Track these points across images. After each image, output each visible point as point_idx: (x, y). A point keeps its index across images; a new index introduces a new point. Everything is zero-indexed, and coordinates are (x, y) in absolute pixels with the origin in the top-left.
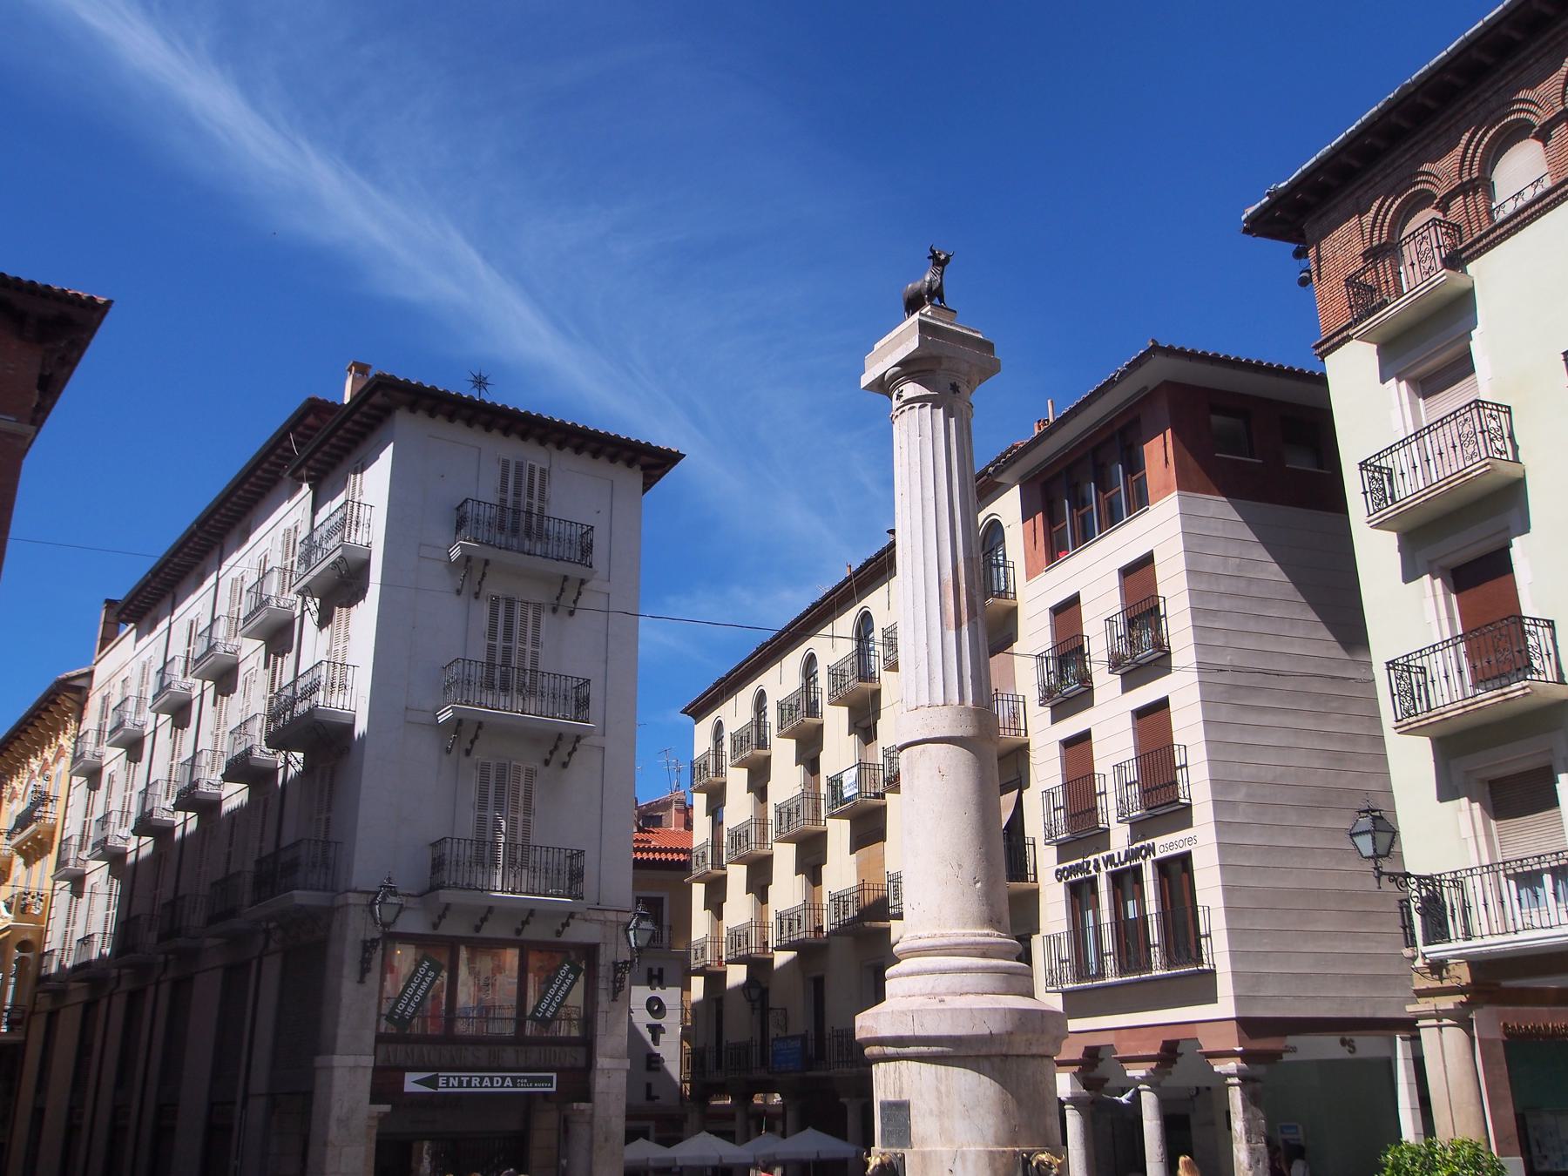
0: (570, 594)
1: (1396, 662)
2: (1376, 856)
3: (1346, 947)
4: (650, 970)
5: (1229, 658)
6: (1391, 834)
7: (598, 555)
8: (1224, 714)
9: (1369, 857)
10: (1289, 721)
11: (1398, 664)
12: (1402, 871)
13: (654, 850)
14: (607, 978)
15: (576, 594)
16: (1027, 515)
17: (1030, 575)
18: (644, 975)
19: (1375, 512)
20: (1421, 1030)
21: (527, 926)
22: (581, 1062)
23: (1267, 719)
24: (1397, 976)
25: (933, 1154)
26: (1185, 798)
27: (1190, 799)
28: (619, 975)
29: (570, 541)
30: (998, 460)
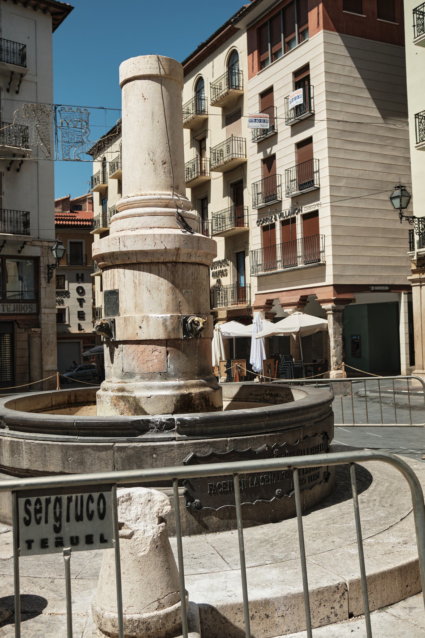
0: (15, 83)
1: (420, 114)
2: (401, 208)
3: (384, 253)
4: (77, 275)
5: (342, 117)
6: (408, 198)
7: (30, 60)
8: (338, 144)
9: (398, 209)
10: (368, 149)
11: (420, 116)
12: (412, 216)
13: (77, 220)
14: (45, 272)
15: (18, 82)
16: (250, 52)
17: (250, 77)
18: (75, 278)
19: (418, 36)
20: (413, 288)
21: (3, 248)
22: (34, 311)
23: (358, 148)
24: (405, 267)
25: (130, 318)
26: (317, 185)
27: (319, 185)
28: (50, 271)
29: (14, 52)
30: (236, 15)
